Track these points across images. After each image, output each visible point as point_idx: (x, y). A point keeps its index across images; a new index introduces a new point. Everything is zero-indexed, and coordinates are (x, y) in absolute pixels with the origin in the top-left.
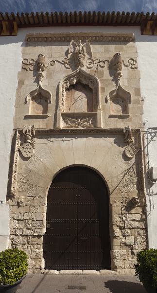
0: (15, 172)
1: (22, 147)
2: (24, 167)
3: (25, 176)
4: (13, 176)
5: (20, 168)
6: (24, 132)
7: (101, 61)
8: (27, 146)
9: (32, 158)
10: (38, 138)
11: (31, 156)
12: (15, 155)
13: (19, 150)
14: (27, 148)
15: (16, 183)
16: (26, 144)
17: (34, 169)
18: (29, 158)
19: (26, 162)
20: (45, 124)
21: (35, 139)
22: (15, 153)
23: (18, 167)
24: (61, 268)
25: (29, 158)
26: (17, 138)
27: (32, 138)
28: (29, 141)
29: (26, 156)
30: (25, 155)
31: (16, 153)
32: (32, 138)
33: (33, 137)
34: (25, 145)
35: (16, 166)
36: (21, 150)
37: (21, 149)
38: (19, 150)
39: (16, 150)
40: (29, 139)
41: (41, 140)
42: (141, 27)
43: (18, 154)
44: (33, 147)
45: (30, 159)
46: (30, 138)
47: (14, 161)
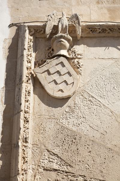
0: (26, 140)
1: (45, 68)
2: (51, 127)
3: (56, 151)
4: (20, 151)
5: (40, 129)
6: (48, 30)
7: (53, 74)
8: (59, 68)
9: (78, 99)
10: (89, 46)
11: (74, 93)
12: (23, 91)
13: (36, 81)
14: (58, 72)
15: (30, 172)
16: (55, 61)
17: (84, 129)
18: (66, 99)
19: (57, 111)
20: (106, 11)
21: (79, 49)
22: (24, 85)
23: (31, 125)
24: (23, 35)
25: (66, 99)
26: (26, 46)
27: (71, 46)
28: (64, 52)
29: (59, 95)
30: (52, 90)
31: (27, 86)
32: (71, 46)
33: (75, 41)
34: (52, 65)
35: (27, 121)
36: (43, 78)
37: (40, 76)
38: (36, 81)
39: (25, 79)
40: (64, 47)
41: (100, 51)
42: (20, 109)
43: (31, 87)
44: (77, 67)
45: (70, 102)
46: (67, 45)
47: (22, 107)
